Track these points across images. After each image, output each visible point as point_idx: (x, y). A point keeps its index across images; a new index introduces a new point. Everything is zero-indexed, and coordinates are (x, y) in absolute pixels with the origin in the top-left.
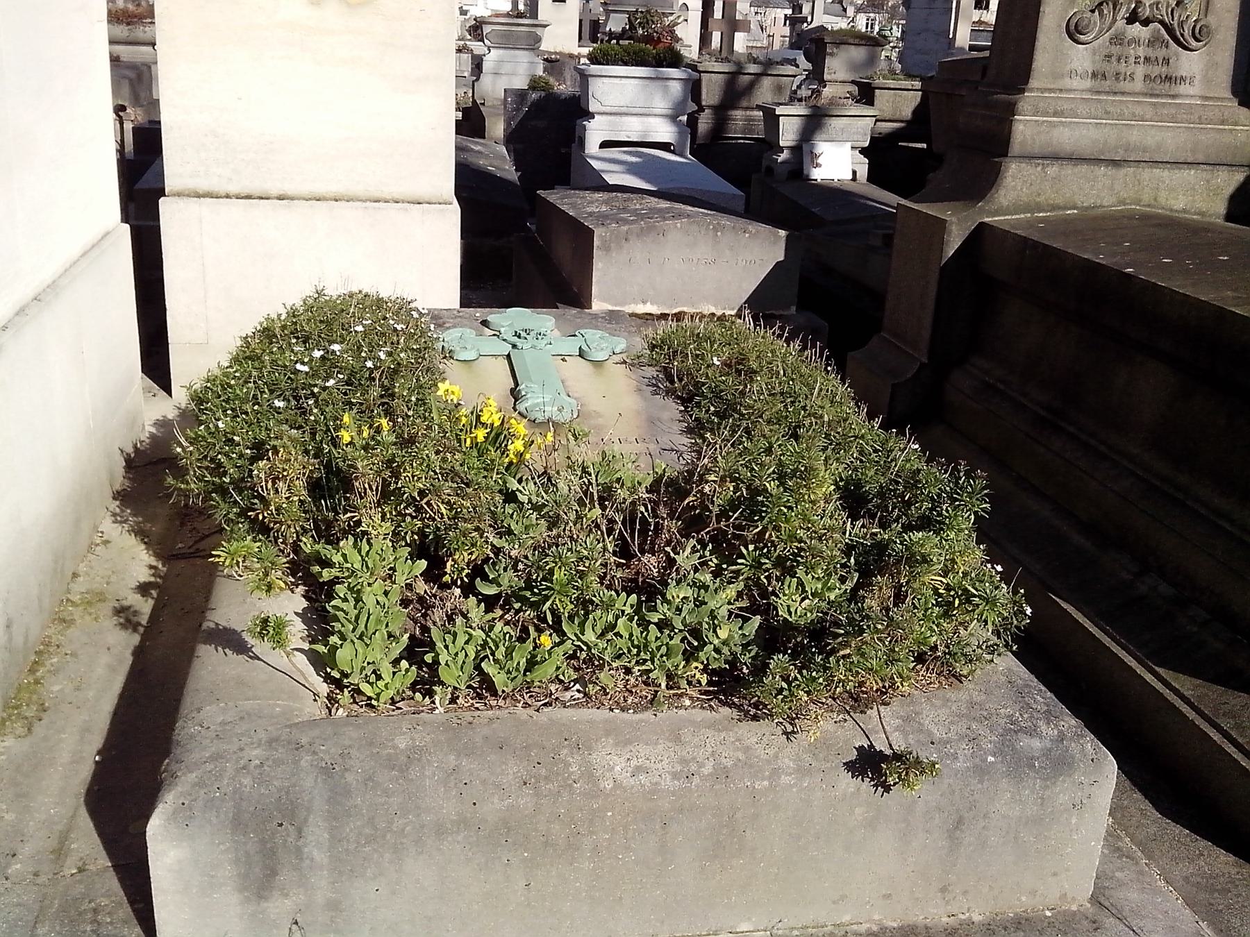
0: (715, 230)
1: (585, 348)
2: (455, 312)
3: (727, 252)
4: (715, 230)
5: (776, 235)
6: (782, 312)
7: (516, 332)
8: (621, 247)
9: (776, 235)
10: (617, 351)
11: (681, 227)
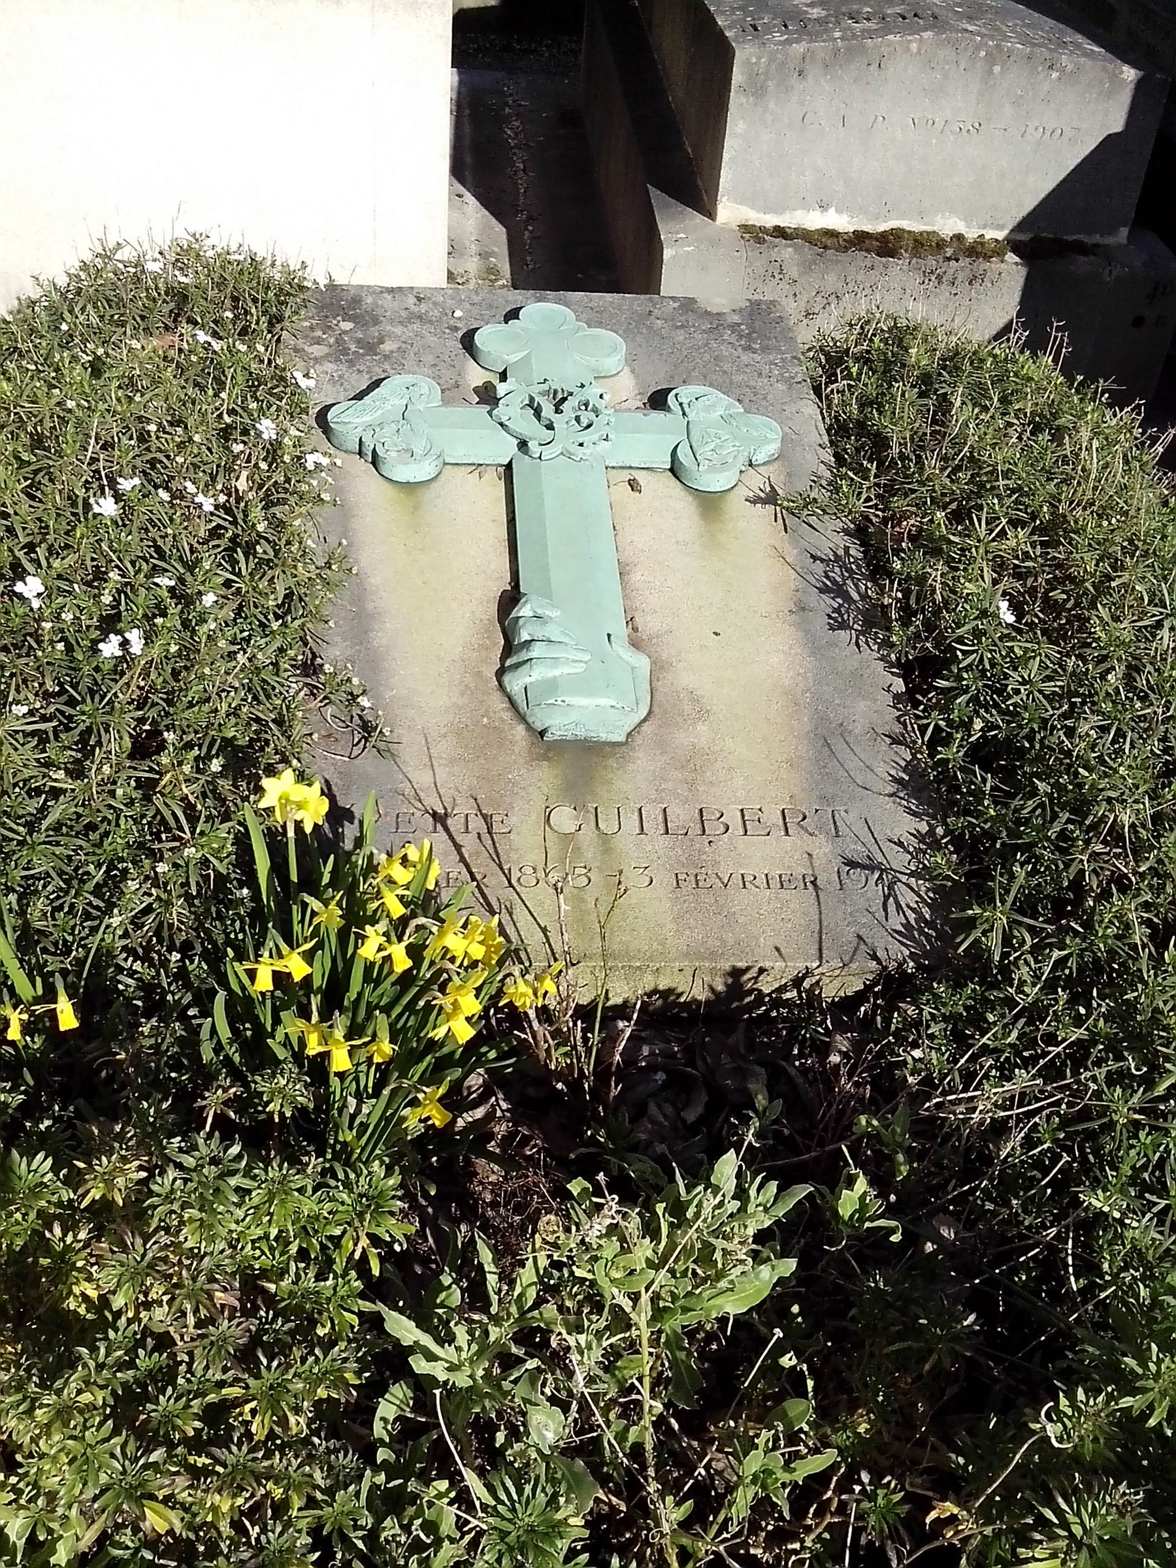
0: (991, 59)
1: (684, 455)
2: (411, 300)
3: (1008, 110)
4: (991, 59)
5: (1115, 78)
6: (1097, 239)
7: (532, 399)
8: (788, 89)
9: (1115, 78)
10: (759, 458)
11: (919, 52)
